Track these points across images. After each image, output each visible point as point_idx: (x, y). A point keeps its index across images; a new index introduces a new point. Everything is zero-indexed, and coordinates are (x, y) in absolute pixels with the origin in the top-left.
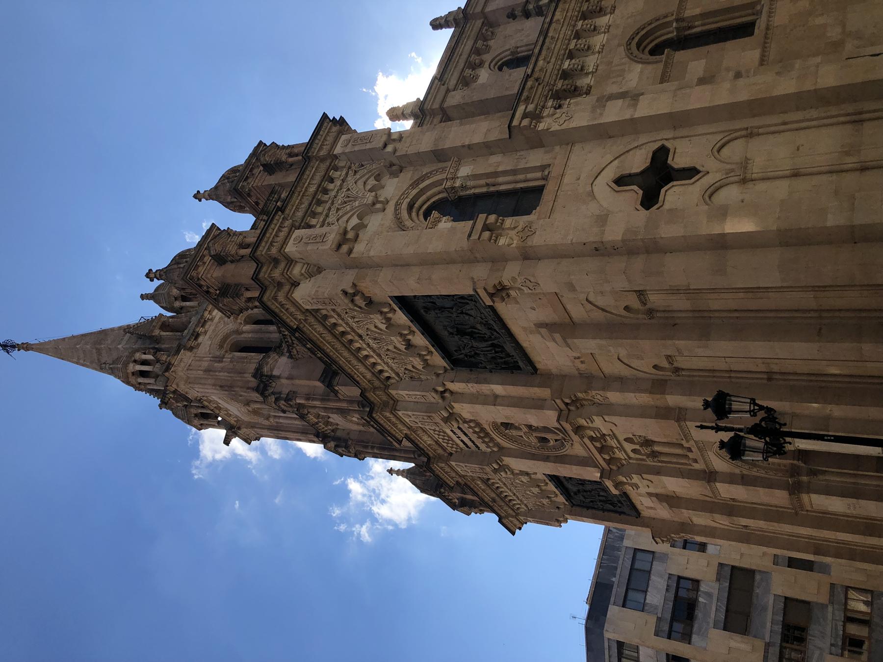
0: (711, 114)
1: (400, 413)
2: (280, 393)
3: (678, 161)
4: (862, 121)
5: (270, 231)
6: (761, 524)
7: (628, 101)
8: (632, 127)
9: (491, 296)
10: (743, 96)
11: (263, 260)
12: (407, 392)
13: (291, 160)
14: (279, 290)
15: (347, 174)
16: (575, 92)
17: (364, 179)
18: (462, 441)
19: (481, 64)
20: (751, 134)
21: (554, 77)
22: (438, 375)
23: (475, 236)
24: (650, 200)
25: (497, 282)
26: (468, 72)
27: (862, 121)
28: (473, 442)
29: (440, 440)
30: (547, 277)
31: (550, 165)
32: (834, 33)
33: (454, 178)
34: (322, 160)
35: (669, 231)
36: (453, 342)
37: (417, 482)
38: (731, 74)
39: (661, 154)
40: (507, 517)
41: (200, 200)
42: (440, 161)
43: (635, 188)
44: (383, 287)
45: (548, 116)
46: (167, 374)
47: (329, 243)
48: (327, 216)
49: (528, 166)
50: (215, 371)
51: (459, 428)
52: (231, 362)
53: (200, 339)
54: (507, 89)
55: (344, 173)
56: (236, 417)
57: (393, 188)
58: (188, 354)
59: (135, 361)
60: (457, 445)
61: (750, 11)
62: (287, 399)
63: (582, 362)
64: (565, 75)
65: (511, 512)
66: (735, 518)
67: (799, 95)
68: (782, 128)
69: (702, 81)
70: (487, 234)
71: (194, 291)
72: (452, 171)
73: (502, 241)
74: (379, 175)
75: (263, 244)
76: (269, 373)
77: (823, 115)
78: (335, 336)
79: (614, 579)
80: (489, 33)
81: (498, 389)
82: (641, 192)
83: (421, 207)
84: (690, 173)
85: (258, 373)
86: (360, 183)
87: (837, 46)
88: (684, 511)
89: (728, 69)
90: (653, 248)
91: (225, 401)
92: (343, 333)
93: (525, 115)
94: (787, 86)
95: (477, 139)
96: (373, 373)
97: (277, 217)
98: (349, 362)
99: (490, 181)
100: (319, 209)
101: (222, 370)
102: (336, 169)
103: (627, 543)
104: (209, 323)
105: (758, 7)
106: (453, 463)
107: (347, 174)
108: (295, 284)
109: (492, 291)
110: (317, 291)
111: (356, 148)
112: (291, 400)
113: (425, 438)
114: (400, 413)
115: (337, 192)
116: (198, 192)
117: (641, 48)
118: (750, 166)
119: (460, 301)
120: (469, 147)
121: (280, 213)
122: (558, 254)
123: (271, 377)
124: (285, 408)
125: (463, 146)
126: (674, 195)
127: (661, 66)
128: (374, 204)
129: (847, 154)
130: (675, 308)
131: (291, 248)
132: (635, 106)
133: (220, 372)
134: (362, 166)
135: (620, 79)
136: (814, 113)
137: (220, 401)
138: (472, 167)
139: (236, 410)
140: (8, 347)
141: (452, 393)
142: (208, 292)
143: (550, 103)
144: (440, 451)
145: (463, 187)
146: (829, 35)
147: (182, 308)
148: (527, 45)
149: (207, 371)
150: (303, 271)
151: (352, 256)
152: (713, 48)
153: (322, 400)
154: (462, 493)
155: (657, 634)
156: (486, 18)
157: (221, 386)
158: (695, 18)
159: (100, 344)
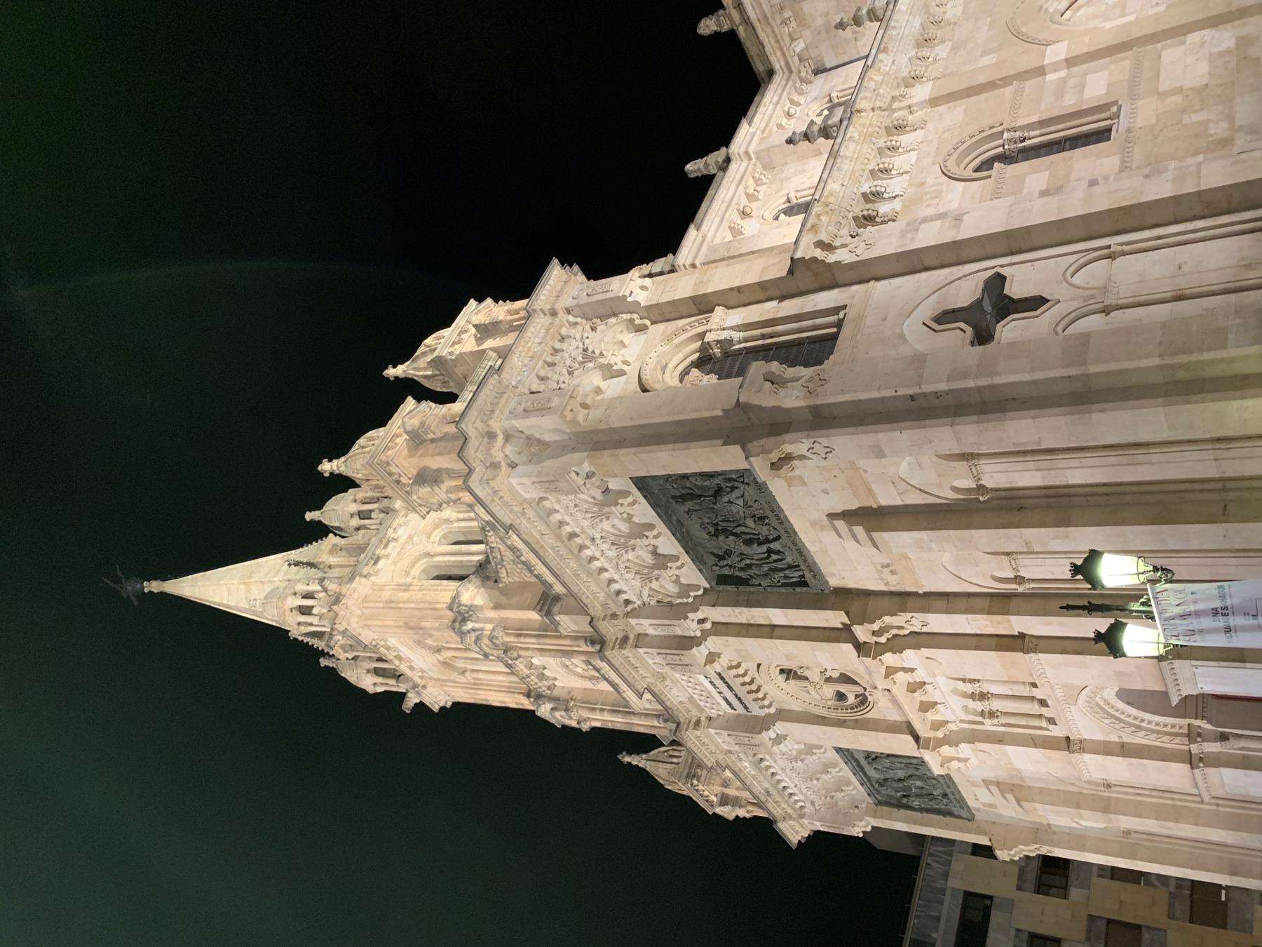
3: (1015, 290)
6: (1151, 825)
24: (983, 337)
31: (845, 307)
38: (1085, 184)
43: (962, 325)
46: (335, 608)
53: (381, 563)
58: (364, 580)
61: (1103, 115)
63: (893, 572)
66: (1112, 816)
71: (381, 482)
76: (468, 603)
79: (935, 935)
87: (1226, 143)
88: (1038, 806)
91: (407, 646)
92: (573, 535)
103: (953, 883)
124: (488, 651)
130: (1020, 484)
132: (958, 227)
137: (401, 647)
142: (398, 482)
146: (1212, 132)
155: (1019, 888)
159: (250, 577)
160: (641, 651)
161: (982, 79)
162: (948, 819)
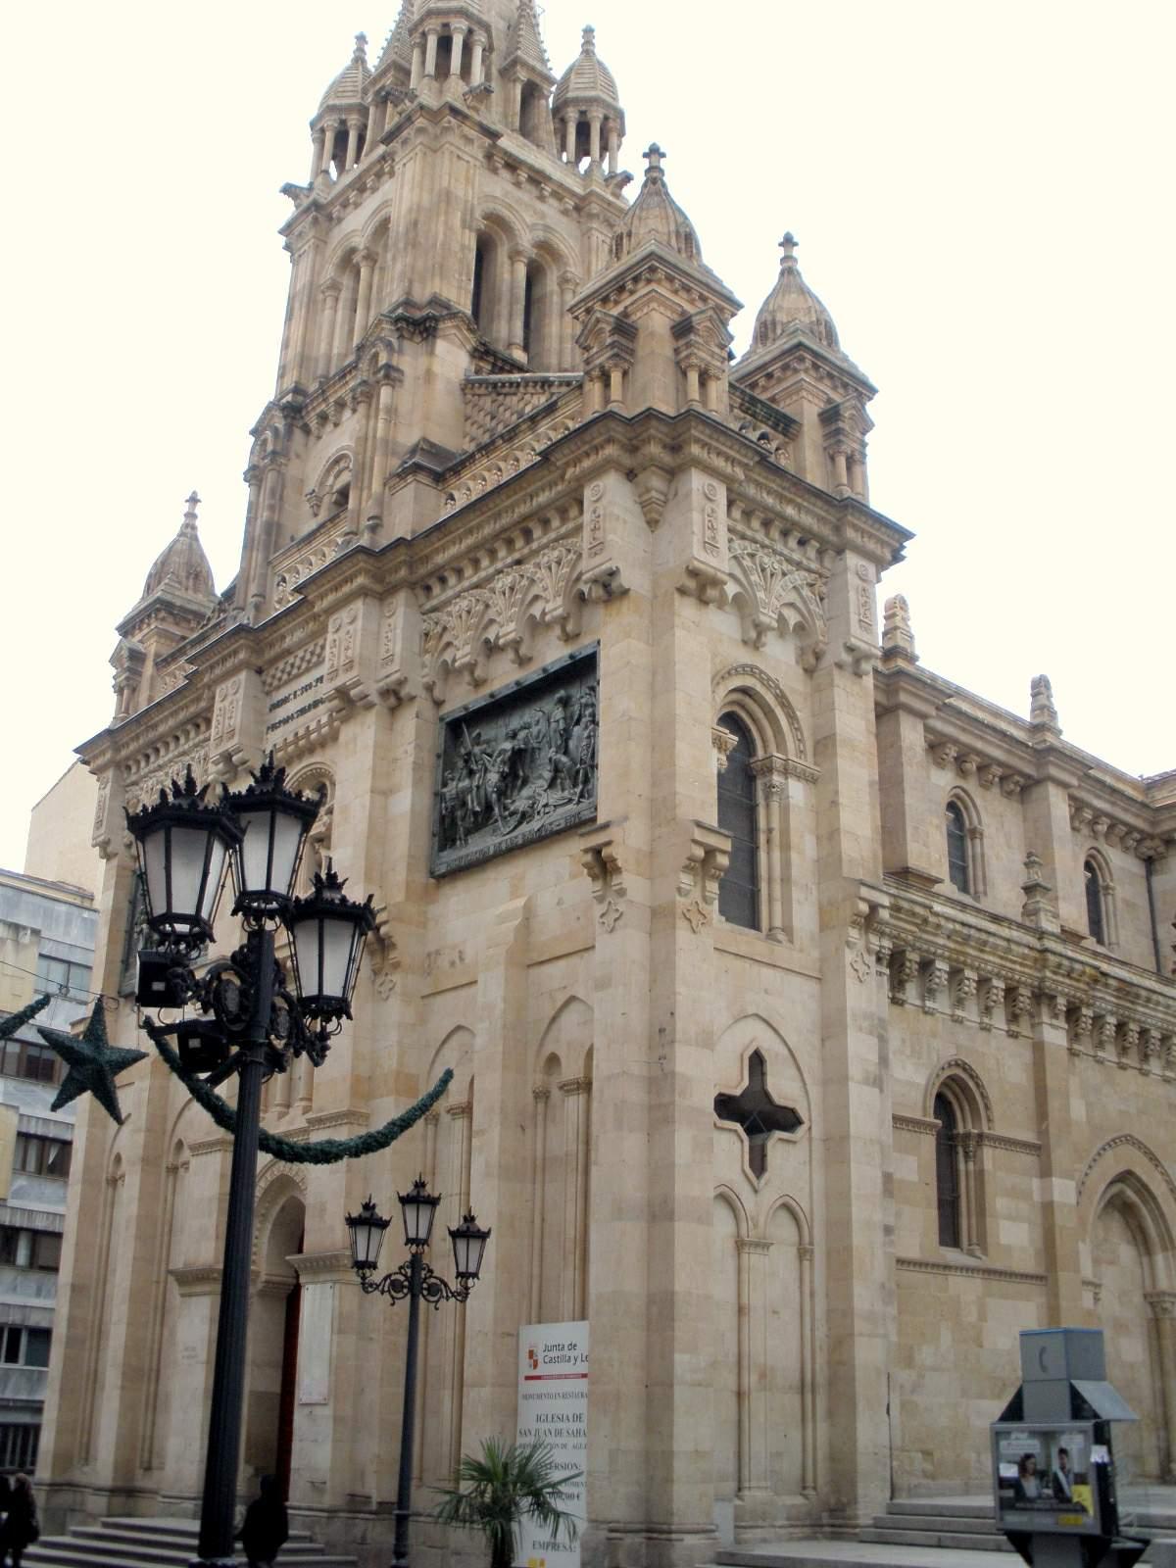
0: (838, 1195)
4: (803, 1393)
7: (873, 1069)
8: (835, 1079)
10: (858, 1239)
14: (623, 447)
15: (809, 570)
16: (897, 983)
17: (799, 604)
18: (285, 700)
19: (962, 773)
20: (803, 1253)
21: (925, 947)
23: (698, 835)
26: (953, 752)
27: (803, 1393)
28: (286, 721)
29: (291, 660)
30: (624, 948)
31: (791, 941)
32: (925, 1355)
35: (683, 1141)
36: (499, 738)
38: (891, 1221)
39: (787, 1120)
42: (817, 743)
43: (746, 1083)
44: (619, 644)
45: (868, 942)
47: (702, 556)
48: (743, 537)
49: (795, 906)
50: (447, 213)
54: (916, 828)
55: (814, 566)
56: (340, 220)
59: (470, 32)
60: (278, 688)
61: (974, 1240)
63: (453, 964)
64: (926, 966)
67: (848, 1313)
68: (807, 1291)
69: (888, 1178)
70: (700, 853)
77: (818, 1344)
80: (1012, 786)
82: (738, 1092)
84: (758, 1163)
86: (793, 597)
87: (908, 1360)
89: (898, 1215)
90: (659, 1116)
92: (527, 534)
93: (874, 907)
94: (864, 1296)
98: (470, 532)
99: (776, 835)
100: (756, 524)
101: (448, 228)
102: (820, 553)
104: (535, 192)
105: (978, 1253)
107: (809, 570)
108: (631, 475)
110: (618, 518)
113: (299, 635)
117: (950, 1082)
118: (759, 1250)
119: (580, 775)
120: (835, 803)
122: (660, 968)
125: (837, 793)
126: (731, 1144)
127: (918, 1115)
129: (763, 1376)
132: (866, 1081)
133: (446, 222)
134: (822, 599)
135: (908, 1052)
136: (821, 1332)
138: (801, 804)
142: (621, 289)
143: (887, 943)
145: (769, 788)
147: (563, 121)
148: (983, 855)
149: (447, 197)
150: (654, 494)
152: (932, 1193)
154: (157, 655)
156: (1038, 782)
157: (416, 223)
158: (979, 1162)
160: (368, 797)
161: (1054, 1104)
162: (118, 966)
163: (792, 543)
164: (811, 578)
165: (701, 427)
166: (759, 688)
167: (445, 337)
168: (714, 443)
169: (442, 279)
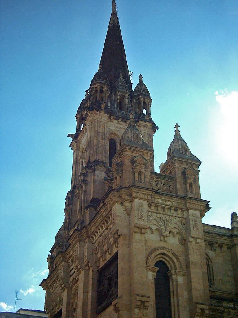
1: (78, 243)
2: (87, 176)
5: (144, 191)
9: (115, 305)
11: (130, 189)
12: (87, 247)
13: (188, 185)
22: (96, 263)
23: (138, 298)
25: (120, 309)
33: (177, 275)
34: (186, 205)
37: (61, 232)
40: (47, 283)
41: (175, 127)
47: (138, 222)
51: (75, 272)
52: (102, 145)
53: (115, 122)
57: (173, 242)
62: (84, 181)
65: (49, 285)
70: (139, 303)
72: (180, 273)
73: (136, 311)
74: (180, 233)
75: (137, 189)
78: (97, 227)
81: (90, 294)
83: (164, 258)
85: (97, 162)
86: (175, 225)
95: (194, 285)
96: (93, 232)
97: (151, 192)
99: (175, 293)
106: (63, 264)
108: (122, 204)
109: (117, 306)
111: (191, 222)
112: (84, 183)
114: (78, 243)
115: (169, 215)
116: (179, 126)
121: (154, 193)
123: (94, 170)
128: (163, 236)
131: (137, 202)
133: (97, 140)
139: (84, 141)
140: (114, 1)
141: (89, 269)
144: (68, 257)
149: (98, 133)
150: (127, 208)
151: (134, 233)
153: (84, 200)
163: (172, 211)
164: (180, 219)
165: (135, 188)
166: (166, 252)
167: (98, 170)
168: (140, 192)
169: (96, 155)
